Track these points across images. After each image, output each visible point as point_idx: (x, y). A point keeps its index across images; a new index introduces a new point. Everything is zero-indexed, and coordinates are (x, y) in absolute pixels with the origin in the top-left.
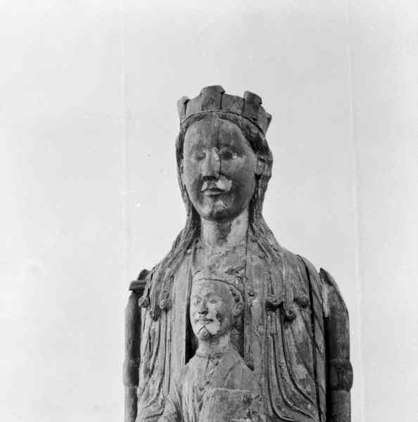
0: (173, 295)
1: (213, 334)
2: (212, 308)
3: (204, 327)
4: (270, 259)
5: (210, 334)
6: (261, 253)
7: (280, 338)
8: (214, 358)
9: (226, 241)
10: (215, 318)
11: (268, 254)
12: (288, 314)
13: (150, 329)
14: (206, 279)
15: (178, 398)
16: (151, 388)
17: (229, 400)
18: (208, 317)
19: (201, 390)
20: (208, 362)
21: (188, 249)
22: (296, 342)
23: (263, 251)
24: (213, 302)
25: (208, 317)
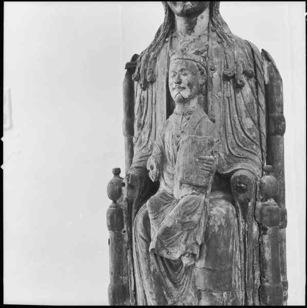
0: (156, 72)
1: (185, 97)
2: (185, 79)
3: (179, 93)
4: (225, 44)
5: (183, 97)
6: (219, 40)
7: (233, 100)
8: (186, 115)
9: (194, 31)
10: (187, 87)
11: (224, 40)
12: (239, 83)
13: (140, 96)
14: (180, 59)
15: (162, 143)
16: (143, 137)
17: (198, 143)
18: (182, 85)
19: (178, 136)
20: (183, 118)
21: (166, 37)
22: (244, 102)
23: (220, 38)
24: (185, 75)
25: (182, 85)
